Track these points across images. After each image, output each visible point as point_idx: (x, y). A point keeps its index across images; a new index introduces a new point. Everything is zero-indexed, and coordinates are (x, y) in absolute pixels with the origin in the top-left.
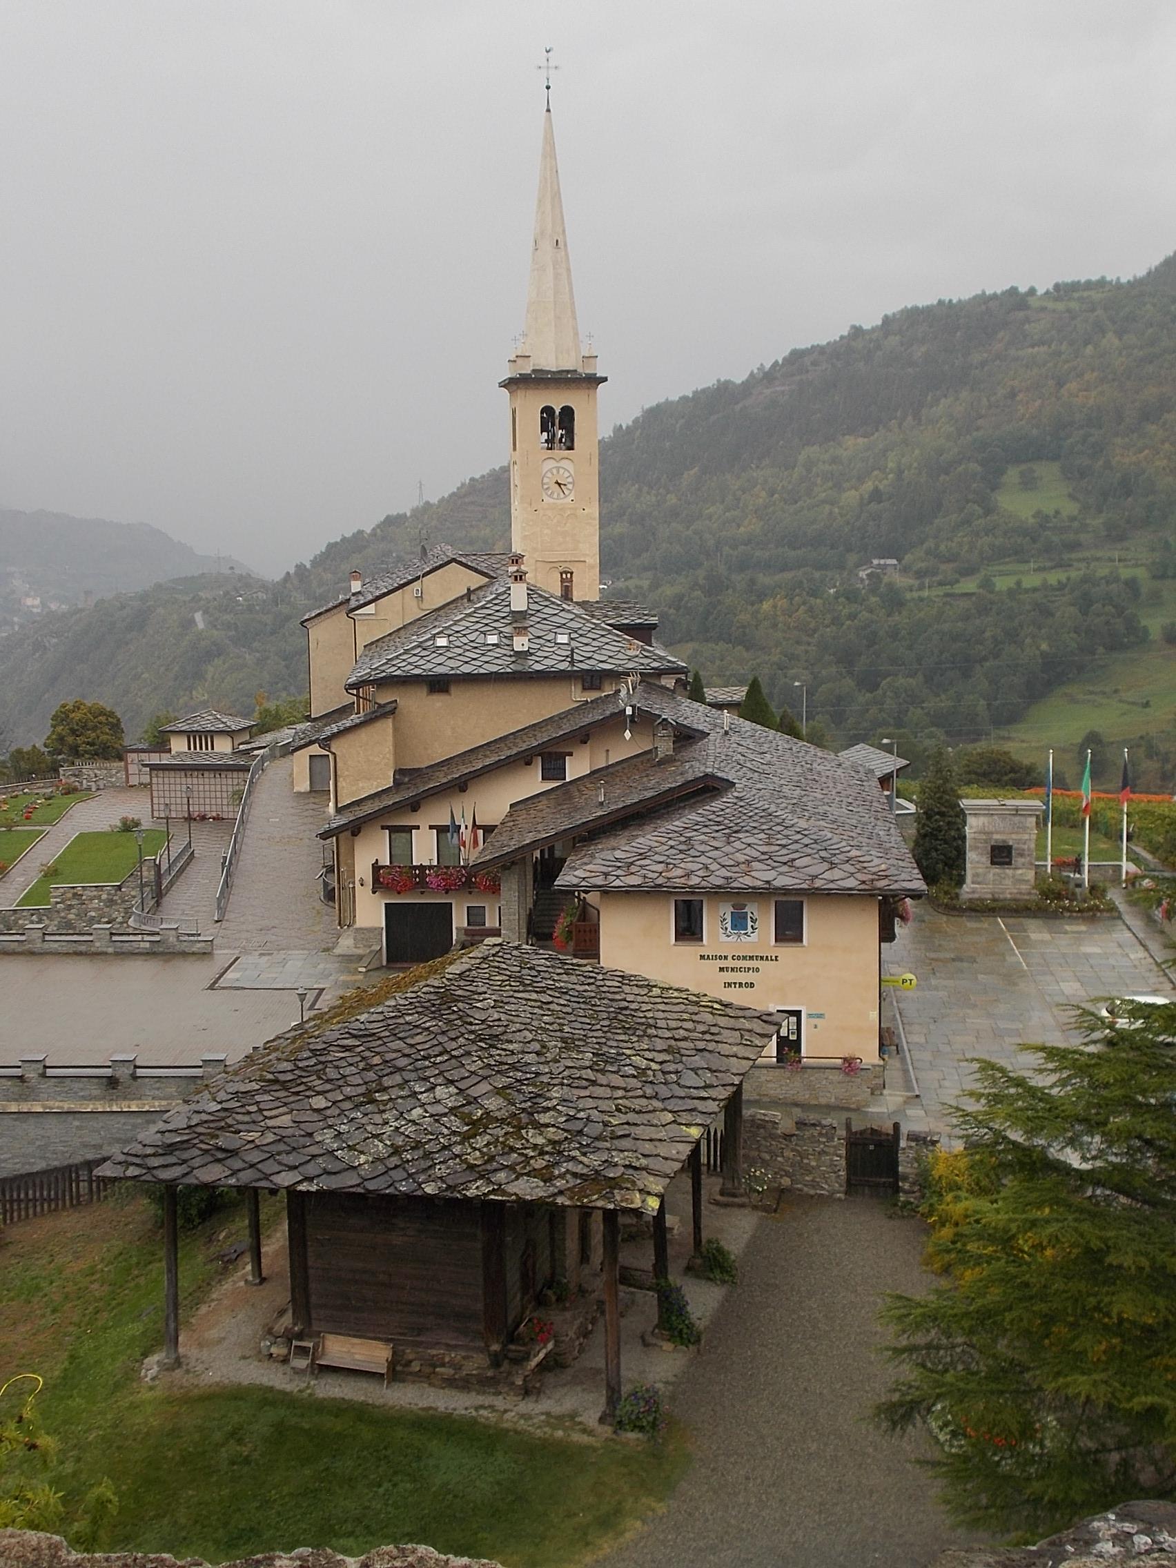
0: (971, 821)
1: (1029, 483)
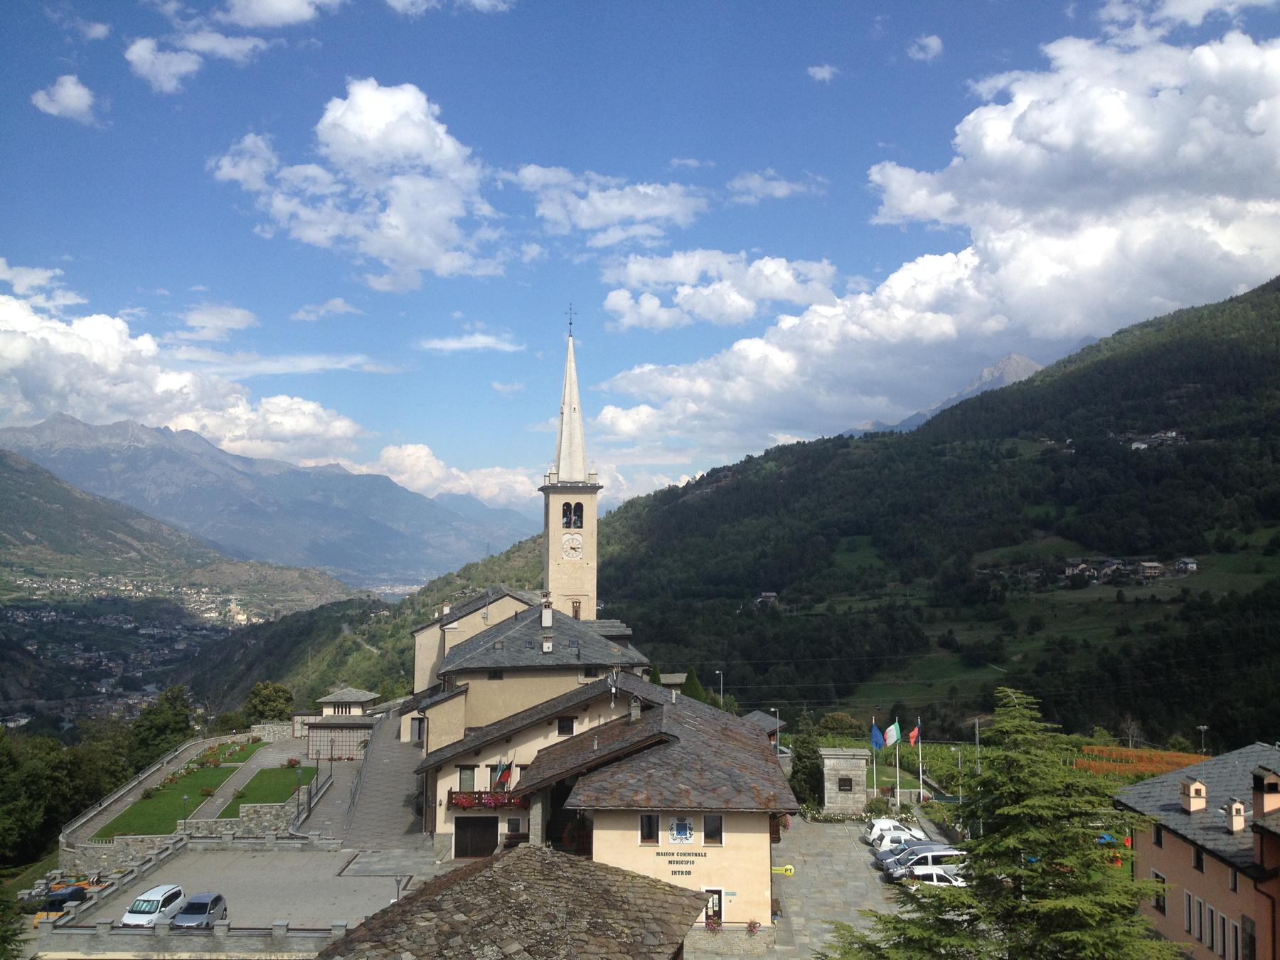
0: (827, 762)
1: (852, 549)
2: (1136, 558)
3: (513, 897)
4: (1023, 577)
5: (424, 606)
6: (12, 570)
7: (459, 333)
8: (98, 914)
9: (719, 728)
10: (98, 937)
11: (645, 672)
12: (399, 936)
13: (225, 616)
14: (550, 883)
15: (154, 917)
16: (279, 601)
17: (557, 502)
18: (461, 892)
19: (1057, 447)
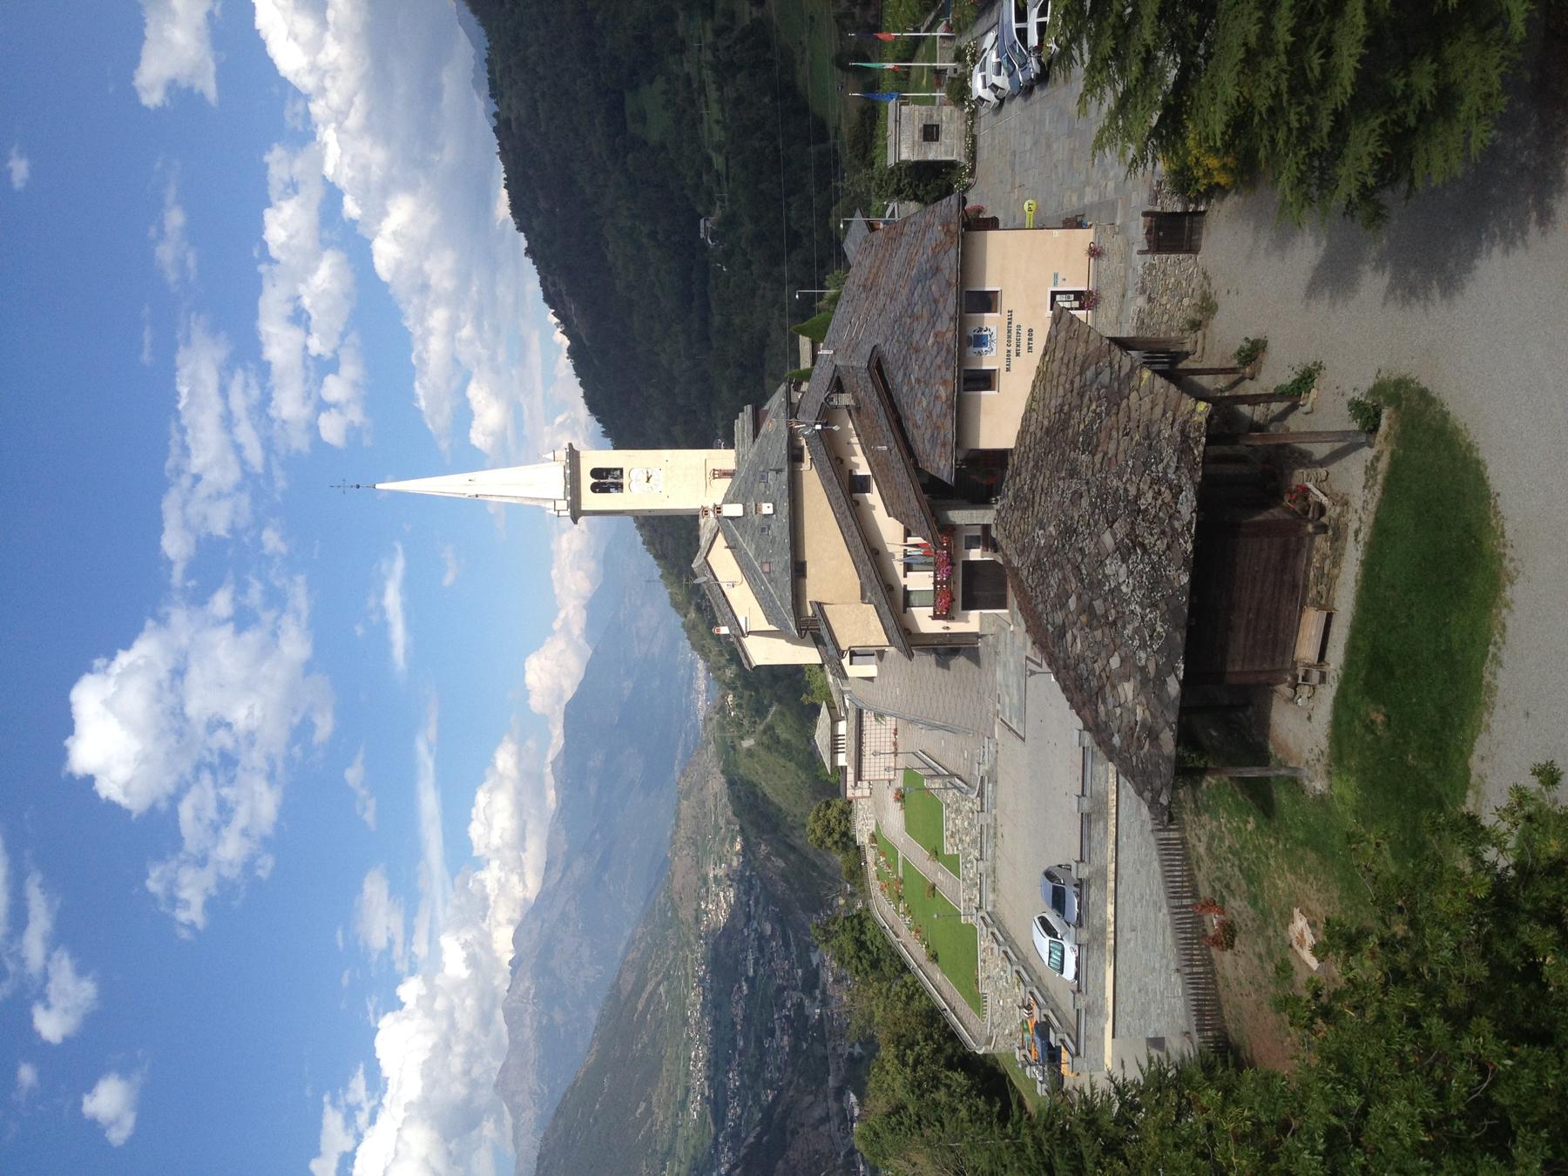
0: (904, 156)
1: (642, 118)
3: (1051, 543)
6: (681, 1125)
7: (385, 626)
8: (1063, 1008)
9: (863, 295)
11: (797, 388)
14: (1037, 499)
15: (1068, 945)
16: (716, 820)
17: (590, 500)
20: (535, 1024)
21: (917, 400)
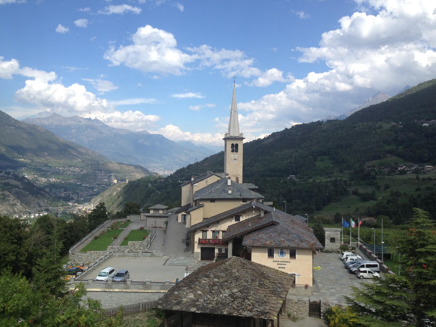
0: (326, 232)
1: (322, 160)
2: (424, 164)
4: (383, 171)
5: (175, 178)
8: (87, 276)
10: (89, 284)
12: (196, 285)
13: (110, 181)
14: (244, 270)
15: (107, 277)
16: (127, 176)
18: (216, 272)
19: (396, 125)
20: (72, 125)
21: (265, 235)
